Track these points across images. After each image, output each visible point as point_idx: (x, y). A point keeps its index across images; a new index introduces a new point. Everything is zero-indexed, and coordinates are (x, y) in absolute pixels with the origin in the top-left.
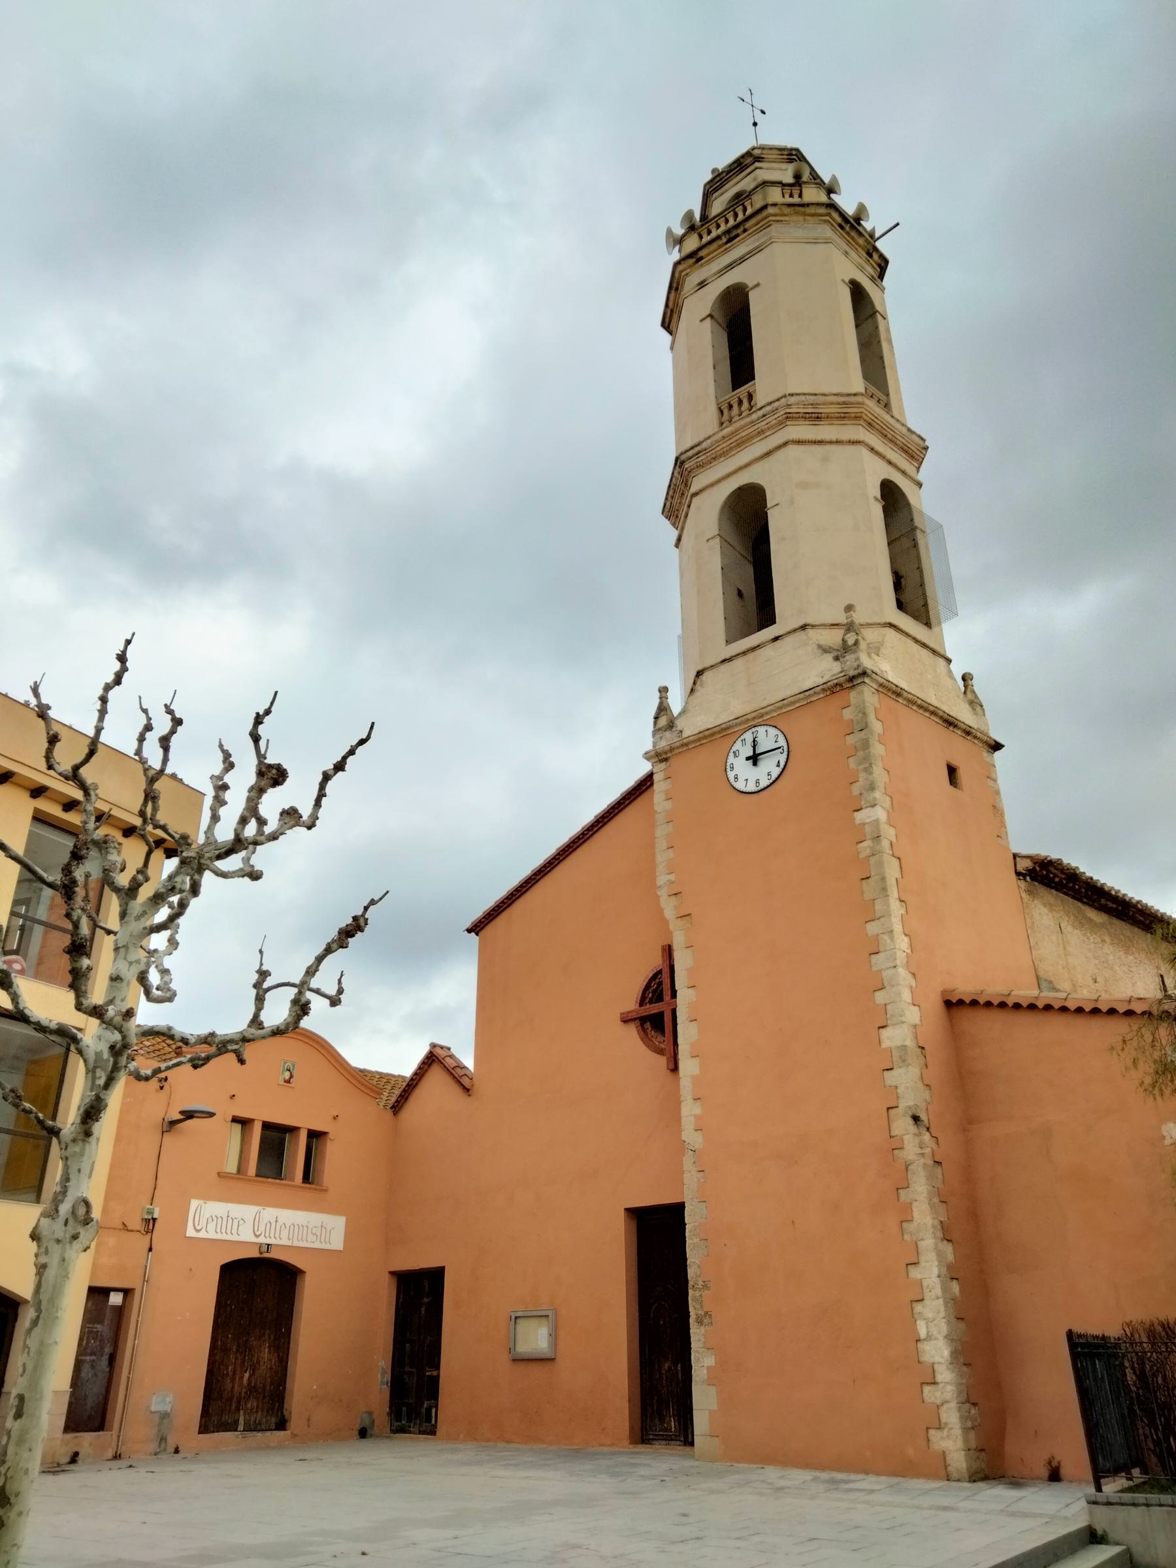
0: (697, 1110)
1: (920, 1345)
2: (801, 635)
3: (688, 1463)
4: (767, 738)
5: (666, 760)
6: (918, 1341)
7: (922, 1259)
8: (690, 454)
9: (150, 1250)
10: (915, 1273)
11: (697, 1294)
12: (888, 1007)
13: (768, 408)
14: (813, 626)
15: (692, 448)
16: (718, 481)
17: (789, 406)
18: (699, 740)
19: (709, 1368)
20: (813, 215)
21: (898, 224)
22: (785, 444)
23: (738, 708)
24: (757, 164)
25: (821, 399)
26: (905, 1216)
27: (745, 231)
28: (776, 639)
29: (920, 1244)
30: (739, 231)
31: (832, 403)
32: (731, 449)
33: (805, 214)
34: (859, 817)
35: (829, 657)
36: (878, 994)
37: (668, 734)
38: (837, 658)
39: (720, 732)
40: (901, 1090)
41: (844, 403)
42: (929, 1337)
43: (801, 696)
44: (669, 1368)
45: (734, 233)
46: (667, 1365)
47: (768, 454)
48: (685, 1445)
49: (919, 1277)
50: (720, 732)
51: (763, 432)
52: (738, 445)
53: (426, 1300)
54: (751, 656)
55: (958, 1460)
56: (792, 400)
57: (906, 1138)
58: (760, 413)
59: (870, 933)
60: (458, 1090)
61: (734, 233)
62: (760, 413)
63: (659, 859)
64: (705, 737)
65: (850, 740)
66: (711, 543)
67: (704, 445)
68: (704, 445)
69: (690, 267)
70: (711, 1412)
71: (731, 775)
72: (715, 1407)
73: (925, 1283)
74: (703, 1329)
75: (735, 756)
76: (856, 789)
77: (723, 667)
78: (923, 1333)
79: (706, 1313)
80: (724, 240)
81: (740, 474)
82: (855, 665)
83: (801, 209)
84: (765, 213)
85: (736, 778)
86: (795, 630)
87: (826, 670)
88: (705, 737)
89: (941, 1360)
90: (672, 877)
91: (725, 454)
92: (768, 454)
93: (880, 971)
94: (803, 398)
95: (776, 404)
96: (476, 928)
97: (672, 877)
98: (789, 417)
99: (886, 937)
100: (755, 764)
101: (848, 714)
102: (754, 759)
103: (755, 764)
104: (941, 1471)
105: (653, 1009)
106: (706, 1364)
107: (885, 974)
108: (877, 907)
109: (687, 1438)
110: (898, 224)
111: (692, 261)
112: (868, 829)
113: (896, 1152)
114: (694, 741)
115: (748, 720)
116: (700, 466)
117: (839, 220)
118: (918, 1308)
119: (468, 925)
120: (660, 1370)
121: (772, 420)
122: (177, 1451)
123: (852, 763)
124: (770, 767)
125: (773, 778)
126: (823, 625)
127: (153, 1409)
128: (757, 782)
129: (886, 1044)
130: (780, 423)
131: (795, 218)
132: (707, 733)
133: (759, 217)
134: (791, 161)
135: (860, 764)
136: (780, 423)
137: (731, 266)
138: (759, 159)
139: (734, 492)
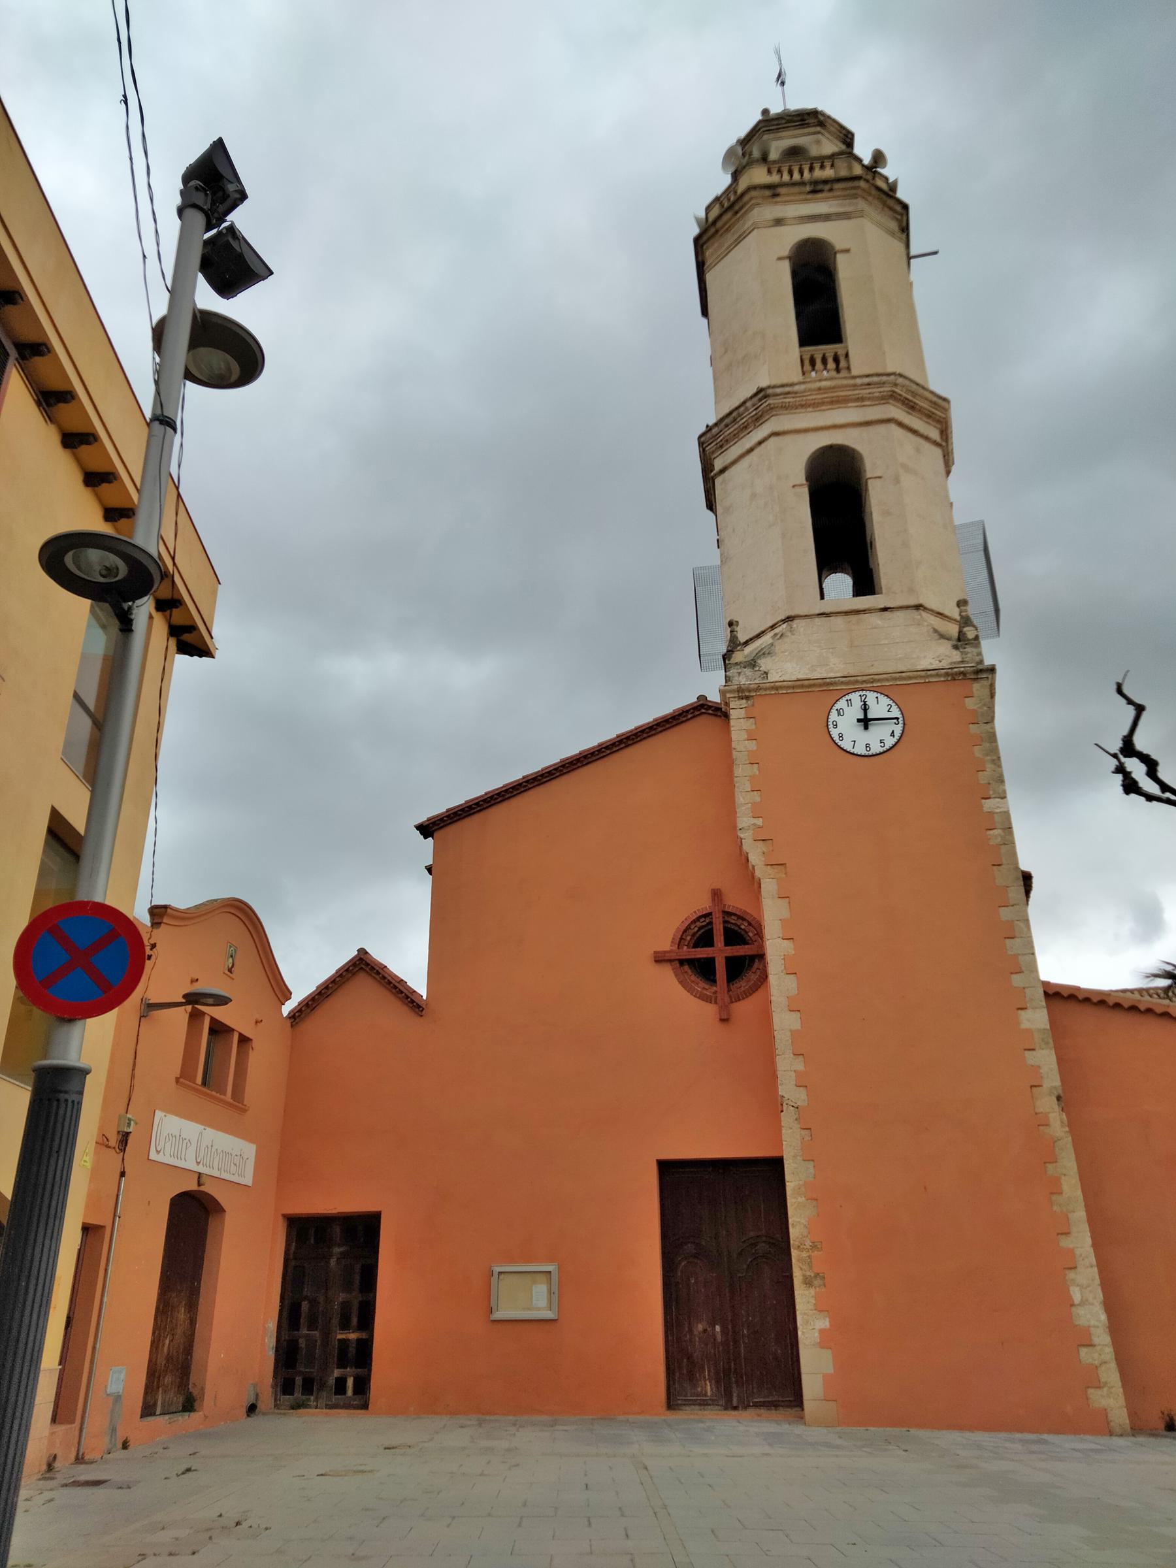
0: (799, 1065)
1: (1073, 1309)
2: (915, 614)
3: (799, 1429)
4: (879, 706)
5: (747, 698)
6: (1072, 1305)
7: (1074, 1229)
8: (779, 390)
9: (123, 1174)
10: (1065, 1243)
11: (805, 1254)
12: (1027, 991)
13: (875, 379)
14: (925, 609)
15: (783, 386)
16: (806, 431)
17: (896, 385)
18: (793, 687)
19: (821, 1331)
20: (891, 209)
21: (936, 253)
22: (889, 421)
23: (836, 667)
24: (818, 129)
25: (921, 391)
26: (1055, 1188)
27: (831, 190)
28: (885, 609)
29: (1070, 1215)
30: (827, 187)
31: (927, 399)
32: (823, 403)
33: (885, 204)
34: (988, 805)
35: (948, 644)
36: (1014, 977)
37: (748, 671)
38: (956, 647)
39: (820, 685)
40: (1044, 1070)
41: (935, 403)
42: (1083, 1303)
43: (923, 673)
44: (705, 1331)
45: (820, 187)
46: (700, 1327)
47: (868, 423)
48: (726, 1409)
49: (1071, 1246)
50: (820, 685)
51: (862, 399)
52: (832, 403)
53: (337, 1250)
54: (854, 618)
55: (1119, 1415)
56: (900, 380)
57: (1051, 1116)
58: (852, 382)
59: (1004, 918)
60: (404, 1010)
61: (820, 187)
62: (852, 382)
63: (740, 799)
64: (802, 686)
65: (973, 729)
66: (798, 489)
67: (796, 388)
68: (796, 388)
69: (764, 198)
70: (825, 1376)
71: (835, 733)
72: (830, 1370)
73: (1078, 1252)
74: (812, 1291)
75: (839, 714)
76: (983, 778)
77: (818, 621)
78: (1077, 1297)
79: (817, 1275)
80: (808, 188)
81: (833, 432)
82: (977, 659)
83: (884, 197)
84: (856, 183)
85: (841, 736)
86: (907, 607)
87: (939, 656)
88: (802, 686)
89: (1097, 1324)
90: (759, 822)
91: (815, 405)
92: (868, 423)
93: (1016, 956)
94: (907, 383)
95: (884, 378)
96: (426, 830)
97: (759, 822)
98: (893, 397)
99: (1021, 924)
100: (866, 728)
101: (970, 703)
102: (865, 722)
103: (866, 728)
104: (1100, 1426)
105: (702, 953)
106: (817, 1327)
107: (1021, 958)
108: (1011, 895)
109: (797, 1400)
110: (936, 253)
111: (768, 193)
112: (997, 818)
113: (1041, 1128)
114: (788, 687)
115: (857, 682)
116: (786, 407)
117: (729, 214)
118: (1071, 1275)
119: (422, 818)
120: (690, 1331)
121: (876, 392)
122: (125, 1446)
123: (978, 752)
124: (879, 738)
125: (887, 747)
126: (932, 610)
127: (109, 1391)
128: (867, 746)
129: (1025, 1025)
130: (883, 398)
131: (876, 202)
132: (806, 682)
133: (850, 184)
134: (844, 142)
135: (987, 755)
136: (883, 398)
137: (826, 218)
138: (821, 124)
139: (822, 448)
